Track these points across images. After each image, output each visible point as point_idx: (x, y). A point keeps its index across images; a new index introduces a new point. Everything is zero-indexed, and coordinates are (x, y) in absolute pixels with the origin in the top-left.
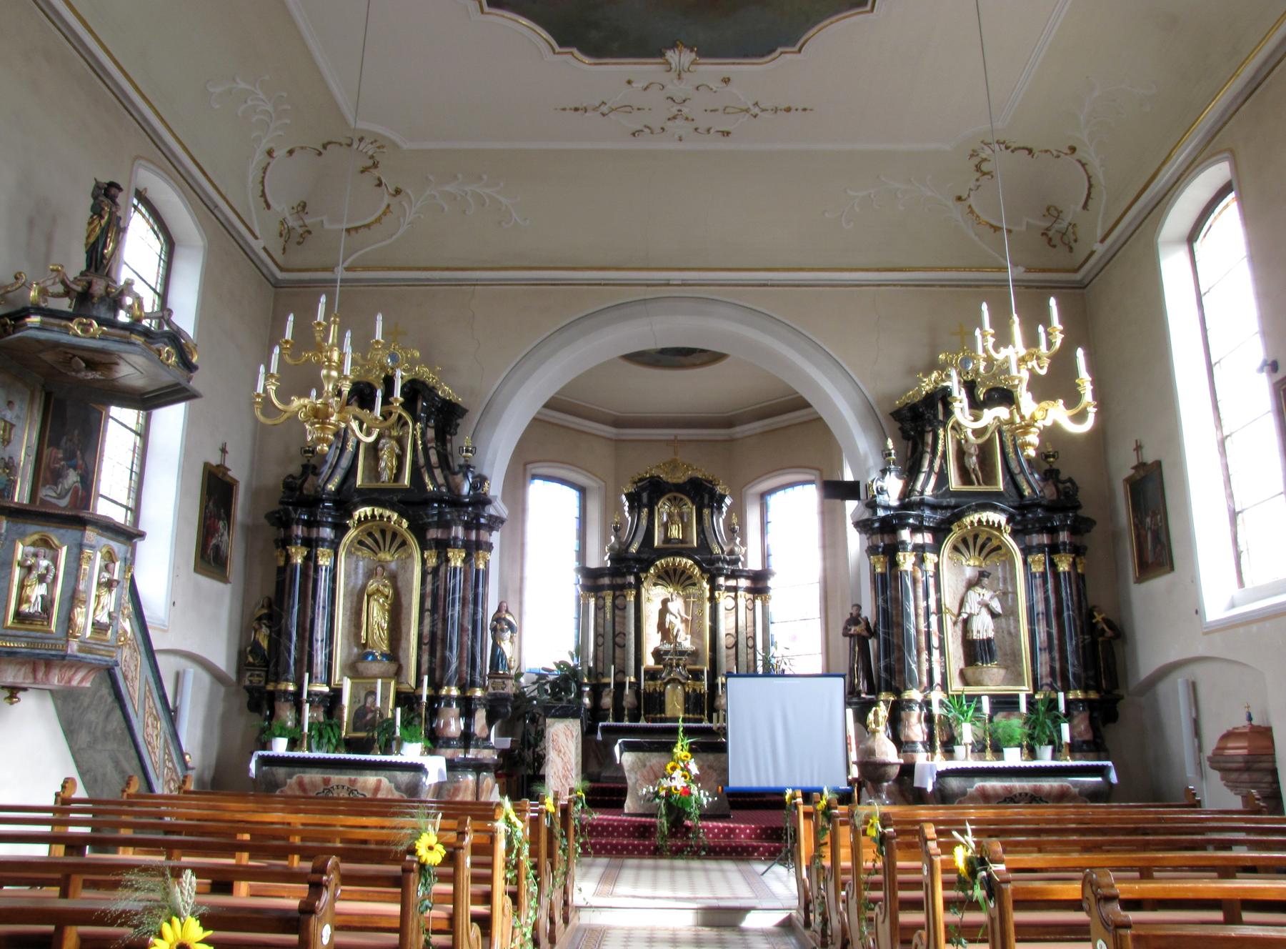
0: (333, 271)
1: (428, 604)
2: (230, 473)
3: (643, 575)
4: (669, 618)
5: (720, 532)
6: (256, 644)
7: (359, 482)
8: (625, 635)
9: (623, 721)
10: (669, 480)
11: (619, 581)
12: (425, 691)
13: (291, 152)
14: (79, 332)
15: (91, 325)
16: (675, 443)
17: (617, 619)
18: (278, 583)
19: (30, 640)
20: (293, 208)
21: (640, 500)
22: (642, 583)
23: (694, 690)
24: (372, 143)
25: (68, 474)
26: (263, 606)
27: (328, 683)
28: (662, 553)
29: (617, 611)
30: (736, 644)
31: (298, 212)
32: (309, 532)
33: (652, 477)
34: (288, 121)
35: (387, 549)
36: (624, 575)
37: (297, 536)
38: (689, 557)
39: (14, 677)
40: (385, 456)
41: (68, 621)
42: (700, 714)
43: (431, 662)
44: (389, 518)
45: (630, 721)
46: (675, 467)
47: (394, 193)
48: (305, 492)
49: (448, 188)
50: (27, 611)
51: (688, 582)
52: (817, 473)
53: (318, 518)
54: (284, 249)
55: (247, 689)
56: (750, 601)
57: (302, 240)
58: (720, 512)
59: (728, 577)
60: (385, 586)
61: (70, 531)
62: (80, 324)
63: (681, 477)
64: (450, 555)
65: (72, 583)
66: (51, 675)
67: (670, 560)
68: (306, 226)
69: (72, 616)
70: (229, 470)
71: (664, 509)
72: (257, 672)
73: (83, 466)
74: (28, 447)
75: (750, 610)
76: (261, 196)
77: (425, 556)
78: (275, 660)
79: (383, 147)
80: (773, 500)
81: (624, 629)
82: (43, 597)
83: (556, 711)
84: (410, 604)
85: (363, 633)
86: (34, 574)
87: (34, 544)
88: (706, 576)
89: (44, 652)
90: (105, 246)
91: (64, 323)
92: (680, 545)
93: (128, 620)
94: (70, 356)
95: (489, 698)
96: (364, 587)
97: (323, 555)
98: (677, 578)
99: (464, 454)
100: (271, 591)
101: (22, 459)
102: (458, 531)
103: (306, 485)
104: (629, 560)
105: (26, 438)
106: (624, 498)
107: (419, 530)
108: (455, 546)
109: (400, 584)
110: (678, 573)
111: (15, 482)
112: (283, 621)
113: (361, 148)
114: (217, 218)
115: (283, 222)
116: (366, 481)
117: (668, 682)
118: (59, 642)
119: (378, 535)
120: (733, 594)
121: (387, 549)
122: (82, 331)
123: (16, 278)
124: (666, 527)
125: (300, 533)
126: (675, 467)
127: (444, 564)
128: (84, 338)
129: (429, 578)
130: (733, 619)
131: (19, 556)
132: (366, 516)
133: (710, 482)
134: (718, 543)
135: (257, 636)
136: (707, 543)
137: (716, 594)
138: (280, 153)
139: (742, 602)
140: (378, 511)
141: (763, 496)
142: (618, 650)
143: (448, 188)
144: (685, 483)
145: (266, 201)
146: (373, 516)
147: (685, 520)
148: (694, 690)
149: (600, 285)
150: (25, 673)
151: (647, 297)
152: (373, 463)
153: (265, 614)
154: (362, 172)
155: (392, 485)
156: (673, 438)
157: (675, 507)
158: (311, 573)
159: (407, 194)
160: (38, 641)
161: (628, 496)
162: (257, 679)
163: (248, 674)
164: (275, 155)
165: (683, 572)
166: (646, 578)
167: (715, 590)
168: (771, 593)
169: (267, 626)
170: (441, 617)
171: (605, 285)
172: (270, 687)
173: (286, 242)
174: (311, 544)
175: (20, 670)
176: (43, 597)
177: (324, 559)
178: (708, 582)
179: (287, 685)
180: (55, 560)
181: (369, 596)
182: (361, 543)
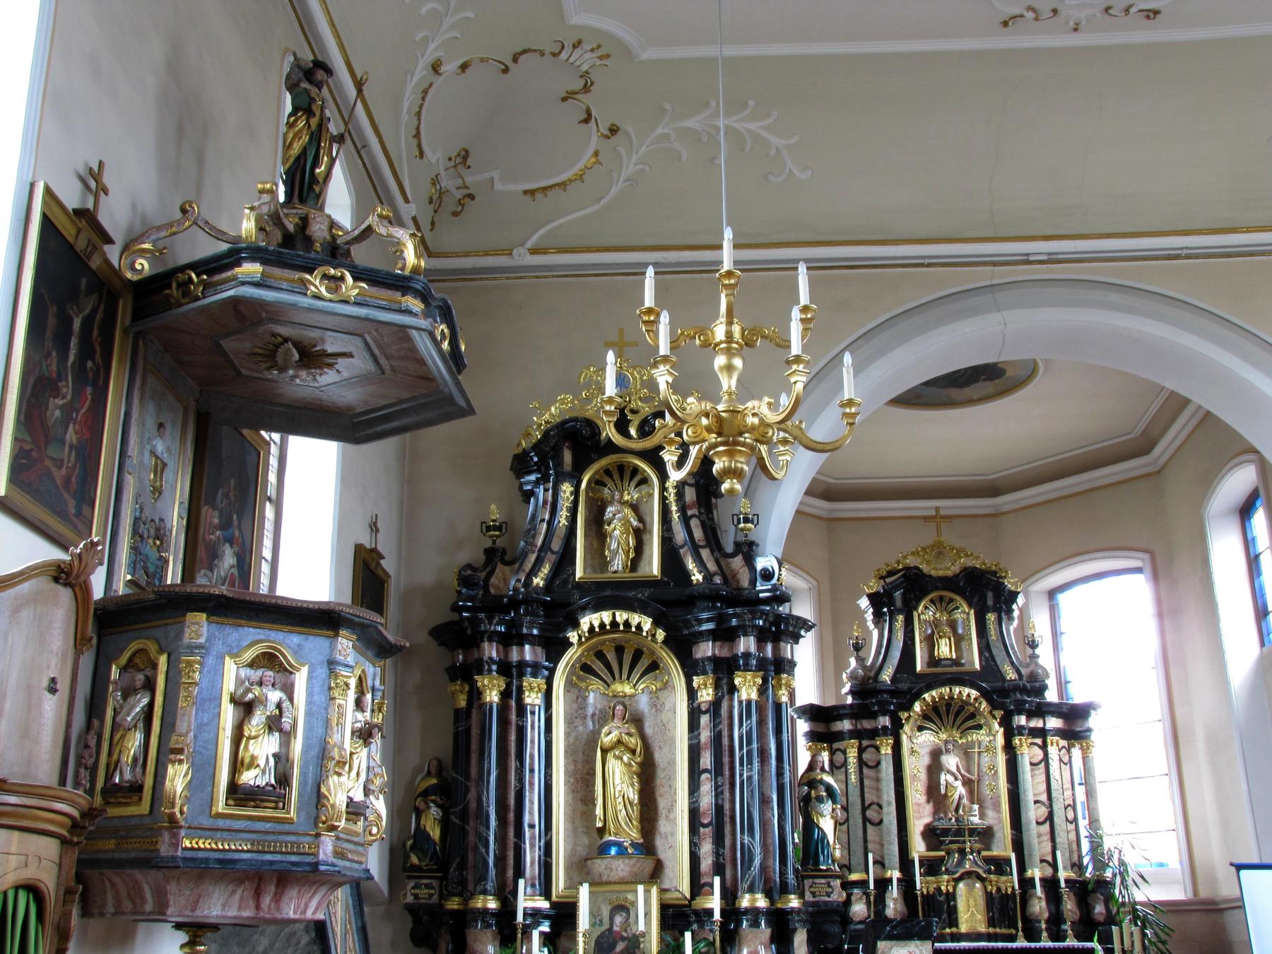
0: (511, 254)
1: (706, 760)
2: (382, 562)
3: (904, 715)
4: (943, 778)
5: (1013, 648)
6: (421, 834)
7: (579, 573)
8: (880, 806)
9: (1039, 941)
10: (933, 573)
11: (867, 724)
12: (714, 903)
13: (464, 67)
14: (323, 289)
15: (342, 279)
16: (937, 519)
17: (866, 782)
18: (456, 736)
19: (253, 836)
20: (450, 159)
21: (891, 603)
22: (902, 726)
23: (999, 889)
24: (592, 50)
25: (224, 551)
26: (429, 773)
27: (547, 894)
28: (931, 681)
29: (865, 770)
30: (1050, 817)
31: (455, 166)
32: (506, 653)
33: (907, 568)
34: (471, 15)
35: (625, 676)
36: (874, 716)
37: (491, 658)
38: (973, 686)
39: (224, 906)
40: (617, 533)
41: (318, 799)
42: (1009, 928)
43: (717, 854)
44: (639, 627)
45: (1079, 937)
46: (940, 553)
47: (608, 133)
48: (492, 591)
49: (691, 123)
50: (252, 783)
51: (970, 723)
52: (1146, 556)
53: (525, 631)
54: (433, 223)
55: (410, 908)
56: (1064, 750)
57: (460, 208)
58: (1011, 619)
59: (1031, 715)
60: (629, 734)
61: (311, 638)
62: (325, 277)
63: (949, 568)
64: (737, 681)
65: (320, 731)
66: (285, 899)
67: (945, 690)
68: (466, 187)
69: (323, 790)
70: (382, 557)
71: (926, 613)
72: (425, 881)
73: (240, 541)
74: (181, 503)
75: (1065, 764)
76: (415, 136)
77: (695, 685)
78: (458, 860)
79: (608, 56)
80: (1062, 598)
81: (879, 797)
82: (275, 755)
83: (894, 928)
84: (672, 763)
85: (599, 811)
86: (258, 719)
87: (252, 665)
88: (999, 714)
89: (278, 857)
90: (316, 163)
91: (297, 275)
92: (955, 669)
93: (381, 797)
94: (280, 339)
95: (810, 909)
96: (594, 738)
97: (531, 689)
98: (951, 718)
99: (742, 525)
100: (443, 746)
101: (175, 523)
102: (746, 644)
103: (493, 580)
104: (882, 692)
105: (179, 488)
106: (864, 603)
107: (681, 646)
108: (747, 668)
109: (649, 730)
110: (954, 709)
111: (167, 562)
112: (472, 795)
113: (572, 60)
114: (364, 164)
115: (435, 181)
116: (589, 570)
117: (961, 878)
118: (302, 839)
119: (611, 657)
120: (1039, 741)
121: (625, 676)
122: (328, 289)
123: (184, 211)
124: (930, 642)
125: (494, 654)
126: (940, 553)
127: (726, 697)
128: (330, 301)
129: (705, 720)
130: (1043, 778)
131: (229, 685)
132: (602, 625)
133: (994, 573)
134: (1012, 663)
135: (422, 822)
136: (996, 664)
137: (1016, 741)
138: (449, 67)
139: (1053, 750)
140: (621, 616)
141: (1052, 594)
142: (870, 829)
143: (691, 123)
144: (956, 576)
145: (419, 146)
146: (614, 624)
147: (960, 631)
148: (999, 889)
149: (922, 265)
150: (242, 898)
151: (995, 282)
152: (595, 543)
153: (433, 785)
154: (564, 99)
155: (628, 576)
156: (933, 513)
157: (941, 612)
158: (513, 717)
159: (628, 134)
160: (270, 838)
161: (872, 597)
162: (421, 892)
163: (412, 884)
164: (443, 69)
165: (961, 709)
166: (908, 719)
167: (1014, 735)
168: (1094, 736)
169: (438, 805)
170: (727, 782)
171: (929, 265)
172: (453, 904)
173: (436, 212)
174: (511, 672)
175: (234, 892)
176: (275, 755)
177: (533, 695)
178: (1000, 725)
179: (485, 901)
180: (289, 690)
181: (605, 751)
182: (586, 668)
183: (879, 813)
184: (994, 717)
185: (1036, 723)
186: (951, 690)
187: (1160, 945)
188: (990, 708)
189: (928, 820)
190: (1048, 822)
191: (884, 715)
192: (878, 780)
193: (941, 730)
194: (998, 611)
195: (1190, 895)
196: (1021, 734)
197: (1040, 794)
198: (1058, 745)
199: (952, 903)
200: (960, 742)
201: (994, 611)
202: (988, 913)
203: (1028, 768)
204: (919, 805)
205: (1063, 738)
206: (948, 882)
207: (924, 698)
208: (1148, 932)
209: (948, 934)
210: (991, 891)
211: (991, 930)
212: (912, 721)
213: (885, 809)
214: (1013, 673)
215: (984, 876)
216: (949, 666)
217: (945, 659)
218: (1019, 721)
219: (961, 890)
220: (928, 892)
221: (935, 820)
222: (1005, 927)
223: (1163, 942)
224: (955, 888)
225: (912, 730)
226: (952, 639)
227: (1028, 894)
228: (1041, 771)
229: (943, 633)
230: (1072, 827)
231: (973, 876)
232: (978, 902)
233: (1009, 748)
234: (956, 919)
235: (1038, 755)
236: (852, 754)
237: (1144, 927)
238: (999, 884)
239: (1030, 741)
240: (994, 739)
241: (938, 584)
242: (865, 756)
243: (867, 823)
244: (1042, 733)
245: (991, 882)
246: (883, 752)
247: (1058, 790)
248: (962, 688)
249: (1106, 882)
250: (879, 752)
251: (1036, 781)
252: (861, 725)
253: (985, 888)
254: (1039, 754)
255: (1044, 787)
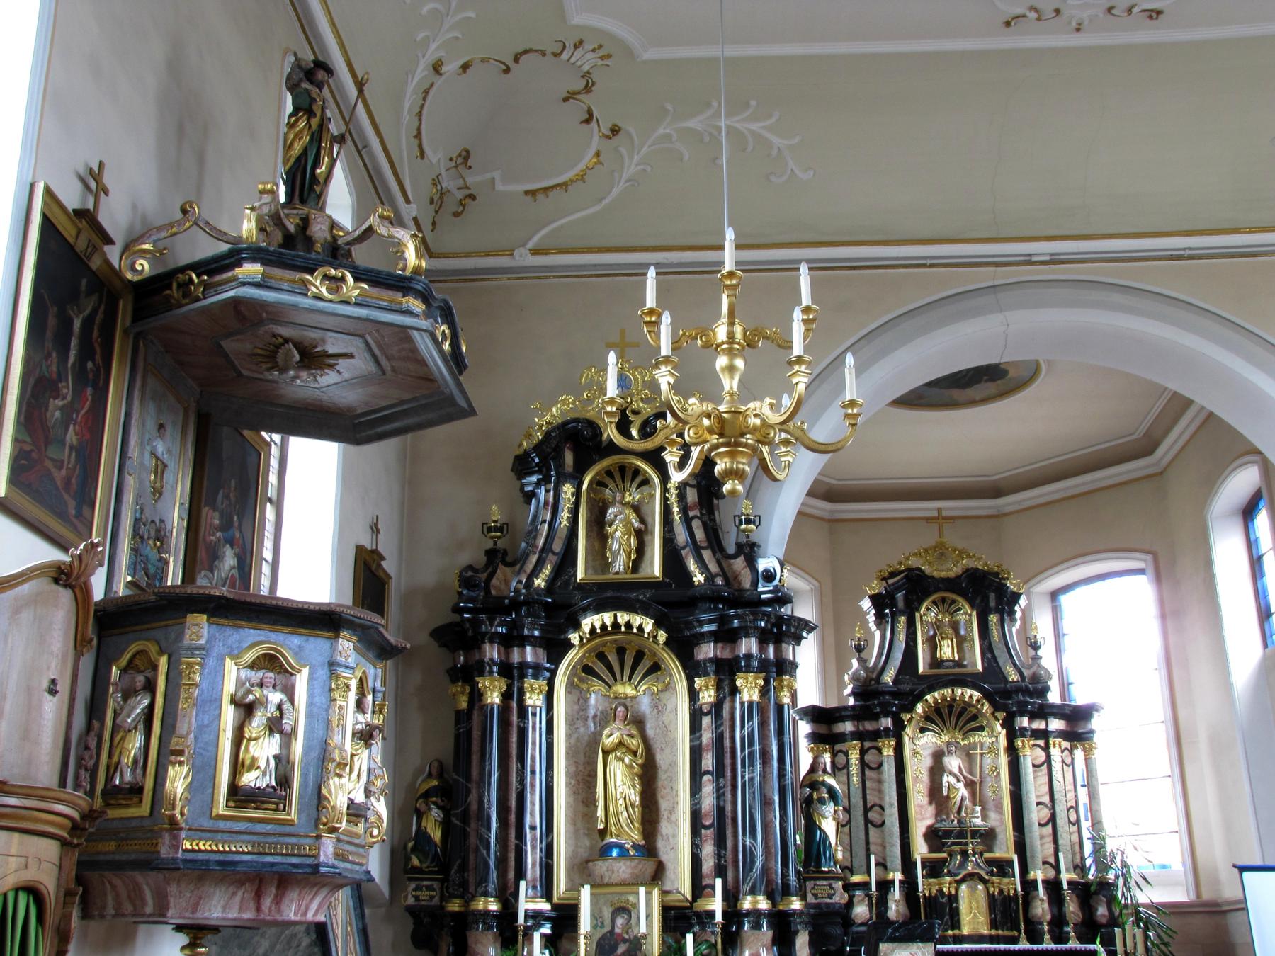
0: (512, 254)
1: (708, 762)
2: (383, 563)
3: (906, 717)
4: (946, 779)
5: (1015, 649)
6: (422, 836)
7: (580, 575)
8: (882, 808)
9: (1042, 943)
10: (935, 574)
11: (869, 726)
12: (716, 905)
13: (465, 67)
14: (324, 290)
15: (343, 279)
16: (939, 520)
17: (868, 784)
18: (457, 737)
19: (254, 838)
20: (451, 159)
21: (893, 604)
22: (904, 728)
23: (1001, 891)
24: (594, 50)
25: (224, 553)
26: (430, 775)
27: (548, 896)
28: (933, 683)
29: (867, 772)
30: (1053, 819)
31: (456, 167)
32: (508, 654)
33: (909, 570)
34: (472, 15)
35: (626, 677)
36: (876, 717)
37: (492, 660)
38: (975, 687)
39: (224, 908)
40: (618, 534)
41: (319, 800)
42: (1012, 930)
43: (719, 856)
44: (640, 628)
45: (1081, 939)
46: (942, 554)
47: (609, 133)
48: (493, 592)
49: (693, 123)
50: (252, 784)
51: (973, 724)
52: (1149, 557)
53: (526, 632)
54: (434, 224)
55: (411, 910)
56: (1066, 752)
57: (461, 208)
58: (1013, 620)
59: (1033, 716)
60: (631, 736)
61: (312, 639)
62: (326, 277)
63: (951, 569)
64: (739, 683)
65: (321, 732)
66: (286, 901)
67: (947, 692)
68: (468, 188)
69: (324, 791)
70: (383, 558)
71: (928, 614)
72: (426, 883)
73: (241, 542)
74: (182, 504)
75: (1068, 766)
76: (416, 137)
77: (697, 686)
78: (459, 862)
79: (609, 56)
80: (1064, 599)
81: (881, 799)
82: (275, 757)
83: (896, 930)
84: (674, 764)
85: (600, 813)
86: (259, 720)
87: (253, 666)
88: (1001, 715)
89: (278, 859)
90: (317, 163)
91: (298, 276)
92: (957, 670)
93: (382, 799)
94: (281, 340)
95: (812, 911)
96: (595, 739)
97: (533, 690)
98: (954, 719)
99: (744, 526)
100: (444, 747)
101: (175, 524)
102: (748, 645)
103: (494, 581)
104: (884, 693)
105: (179, 489)
106: (866, 604)
107: (683, 647)
108: (748, 670)
109: (650, 732)
110: (956, 711)
111: (167, 563)
112: (473, 797)
113: (573, 60)
114: (365, 165)
115: (436, 182)
116: (590, 571)
117: (963, 880)
118: (303, 841)
119: (613, 658)
120: (1041, 743)
121: (626, 677)
122: (328, 290)
123: (184, 211)
124: (933, 644)
125: (495, 656)
126: (942, 554)
127: (728, 699)
128: (331, 301)
129: (706, 721)
130: (1046, 779)
131: (229, 687)
132: (604, 627)
133: (997, 574)
134: (1015, 664)
135: (423, 824)
136: (998, 666)
137: (1019, 742)
138: (450, 68)
139: (1055, 752)
140: (623, 618)
141: (1054, 595)
142: (872, 830)
143: (693, 123)
144: (958, 577)
145: (420, 146)
146: (616, 625)
147: (962, 632)
148: (1001, 891)
149: (924, 266)
150: (242, 900)
151: (997, 283)
152: (597, 545)
153: (434, 787)
154: (566, 100)
155: (629, 577)
156: (935, 514)
157: (943, 613)
158: (515, 718)
159: (629, 135)
160: (270, 839)
161: (874, 598)
162: (422, 894)
163: (413, 886)
164: (444, 69)
165: (964, 710)
166: (910, 720)
167: (1016, 737)
168: (1096, 738)
169: (439, 807)
170: (729, 784)
171: (932, 266)
172: (454, 906)
173: (437, 212)
174: (513, 673)
175: (234, 894)
176: (275, 757)
177: (535, 697)
178: (1003, 726)
179: (486, 903)
180: (289, 692)
181: (606, 753)
182: (587, 670)
183: (882, 815)
184: (997, 719)
185: (1039, 725)
186: (953, 691)
187: (1163, 947)
188: (992, 710)
189: (930, 821)
190: (1050, 824)
191: (886, 716)
192: (880, 781)
193: (943, 731)
194: (1000, 612)
195: (1193, 897)
196: (1023, 736)
197: (1042, 796)
198: (1060, 747)
199: (954, 905)
200: (962, 743)
201: (996, 612)
202: (990, 915)
203: (1030, 769)
204: (921, 806)
205: (1065, 740)
206: (950, 883)
207: (926, 700)
208: (1150, 934)
209: (950, 936)
210: (994, 893)
211: (993, 932)
212: (914, 722)
213: (887, 811)
214: (1015, 674)
215: (987, 877)
216: (951, 667)
217: (947, 661)
218: (1021, 723)
219: (963, 892)
220: (930, 894)
221: (937, 821)
222: (1007, 929)
223: (1166, 944)
224: (957, 890)
225: (914, 732)
226: (954, 640)
227: (1030, 896)
228: (1043, 773)
229: (946, 634)
230: (1074, 828)
231: (976, 878)
232: (980, 904)
233: (1012, 750)
234: (959, 921)
235: (1041, 757)
236: (854, 756)
237: (1146, 929)
238: (1002, 886)
239: (1032, 742)
240: (997, 741)
241: (940, 586)
242: (867, 758)
243: (869, 825)
244: (1044, 734)
245: (993, 883)
246: (885, 754)
247: (1060, 792)
248: (964, 690)
249: (1108, 884)
250: (881, 753)
251: (1039, 782)
252: (863, 726)
253: (988, 890)
254: (1041, 755)
255: (1046, 788)
